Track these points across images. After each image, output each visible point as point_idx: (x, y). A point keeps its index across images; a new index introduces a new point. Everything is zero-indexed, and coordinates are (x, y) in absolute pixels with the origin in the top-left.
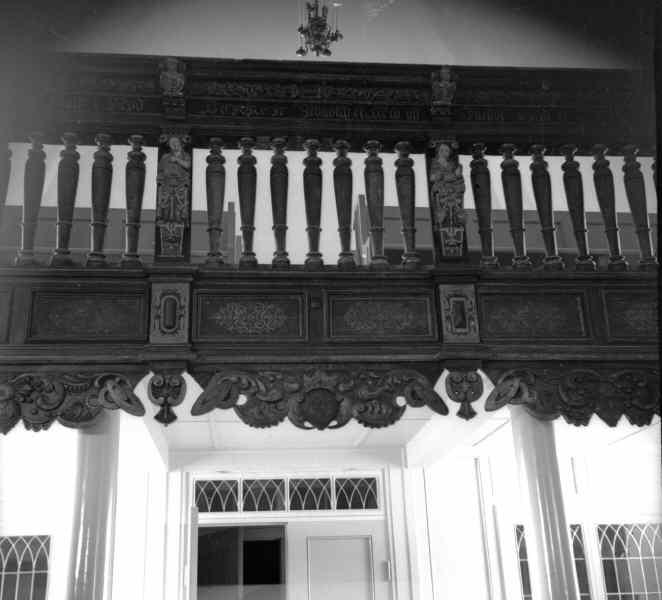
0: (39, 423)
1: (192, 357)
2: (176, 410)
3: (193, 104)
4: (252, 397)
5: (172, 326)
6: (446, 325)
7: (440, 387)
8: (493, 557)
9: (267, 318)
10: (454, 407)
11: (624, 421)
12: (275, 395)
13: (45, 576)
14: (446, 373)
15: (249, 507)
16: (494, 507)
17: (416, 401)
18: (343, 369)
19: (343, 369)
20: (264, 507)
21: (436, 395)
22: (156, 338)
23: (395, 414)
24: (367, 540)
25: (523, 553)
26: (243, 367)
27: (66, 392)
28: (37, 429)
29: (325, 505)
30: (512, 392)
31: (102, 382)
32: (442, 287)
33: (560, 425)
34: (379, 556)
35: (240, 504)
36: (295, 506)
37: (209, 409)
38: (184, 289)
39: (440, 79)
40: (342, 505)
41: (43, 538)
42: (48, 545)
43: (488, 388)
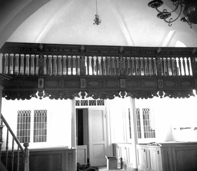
0: (66, 99)
1: (86, 90)
2: (84, 97)
3: (85, 51)
4: (94, 95)
5: (83, 85)
6: (121, 85)
7: (120, 94)
8: (124, 114)
9: (96, 83)
10: (121, 97)
11: (144, 98)
12: (97, 95)
13: (46, 117)
14: (121, 92)
15: (82, 105)
16: (131, 138)
17: (116, 96)
18: (106, 91)
19: (106, 91)
20: (84, 105)
21: (119, 95)
22: (81, 87)
23: (114, 98)
24: (102, 111)
25: (129, 113)
26: (93, 91)
27: (70, 94)
28: (66, 99)
29: (95, 105)
30: (130, 94)
31: (74, 93)
32: (121, 80)
33: (136, 99)
34: (104, 113)
35: (80, 104)
36: (90, 105)
37: (88, 97)
38: (85, 80)
39: (121, 48)
40: (98, 105)
41: (46, 110)
42: (47, 111)
43: (126, 94)
